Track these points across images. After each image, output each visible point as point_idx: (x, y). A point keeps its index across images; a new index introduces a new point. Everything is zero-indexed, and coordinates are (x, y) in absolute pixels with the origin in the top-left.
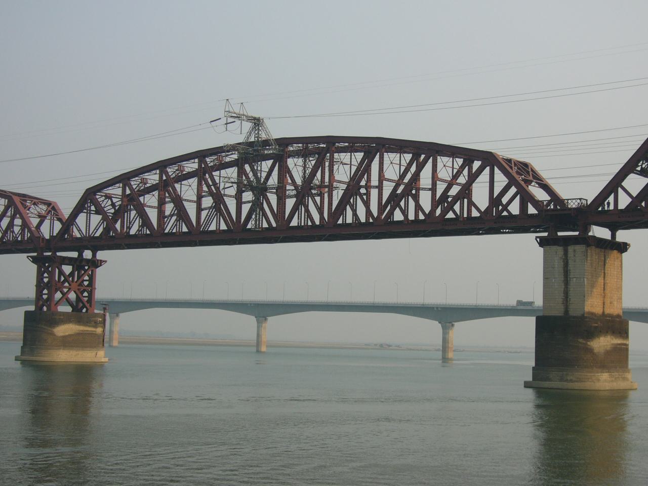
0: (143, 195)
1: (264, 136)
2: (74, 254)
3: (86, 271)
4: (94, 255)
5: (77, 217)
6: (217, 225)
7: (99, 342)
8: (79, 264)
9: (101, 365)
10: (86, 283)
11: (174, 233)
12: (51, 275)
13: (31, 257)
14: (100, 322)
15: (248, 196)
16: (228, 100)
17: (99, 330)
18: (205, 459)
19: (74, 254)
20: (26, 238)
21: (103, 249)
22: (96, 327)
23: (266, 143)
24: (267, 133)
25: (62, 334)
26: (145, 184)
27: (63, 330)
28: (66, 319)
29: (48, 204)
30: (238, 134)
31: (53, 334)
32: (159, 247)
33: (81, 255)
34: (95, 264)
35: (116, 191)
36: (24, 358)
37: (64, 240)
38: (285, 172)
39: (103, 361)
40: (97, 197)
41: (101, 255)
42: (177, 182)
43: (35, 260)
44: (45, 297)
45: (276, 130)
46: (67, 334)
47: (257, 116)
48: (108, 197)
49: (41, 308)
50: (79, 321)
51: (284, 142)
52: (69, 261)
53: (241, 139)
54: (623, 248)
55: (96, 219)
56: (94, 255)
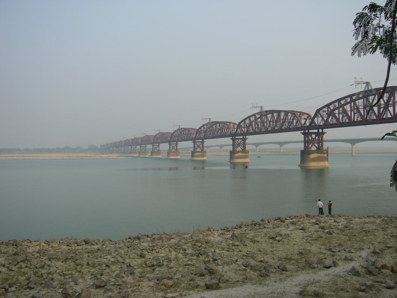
0: (335, 110)
1: (370, 88)
2: (316, 131)
3: (320, 136)
4: (322, 131)
5: (314, 119)
6: (357, 118)
7: (326, 159)
8: (317, 134)
9: (248, 162)
10: (320, 140)
11: (384, 118)
12: (308, 138)
13: (302, 133)
14: (326, 153)
15: (262, 124)
16: (355, 78)
17: (325, 155)
18: (100, 156)
19: (316, 131)
20: (344, 122)
21: (325, 128)
22: (324, 154)
23: (371, 90)
24: (371, 87)
25: (312, 157)
26: (335, 106)
27: (312, 156)
28: (314, 152)
29: (307, 114)
30: (361, 88)
31: (309, 157)
32: (379, 124)
33: (318, 131)
34: (323, 133)
35: (326, 109)
36: (301, 165)
37: (313, 125)
38: (267, 118)
39: (327, 165)
40: (320, 112)
41: (325, 130)
42: (345, 105)
43: (303, 133)
44: (307, 145)
45: (265, 109)
46: (314, 157)
47: (367, 81)
48: (324, 111)
49: (306, 149)
50: (318, 153)
51: (266, 111)
52: (314, 133)
53: (362, 90)
54: (325, 133)
55: (320, 119)
56: (322, 131)
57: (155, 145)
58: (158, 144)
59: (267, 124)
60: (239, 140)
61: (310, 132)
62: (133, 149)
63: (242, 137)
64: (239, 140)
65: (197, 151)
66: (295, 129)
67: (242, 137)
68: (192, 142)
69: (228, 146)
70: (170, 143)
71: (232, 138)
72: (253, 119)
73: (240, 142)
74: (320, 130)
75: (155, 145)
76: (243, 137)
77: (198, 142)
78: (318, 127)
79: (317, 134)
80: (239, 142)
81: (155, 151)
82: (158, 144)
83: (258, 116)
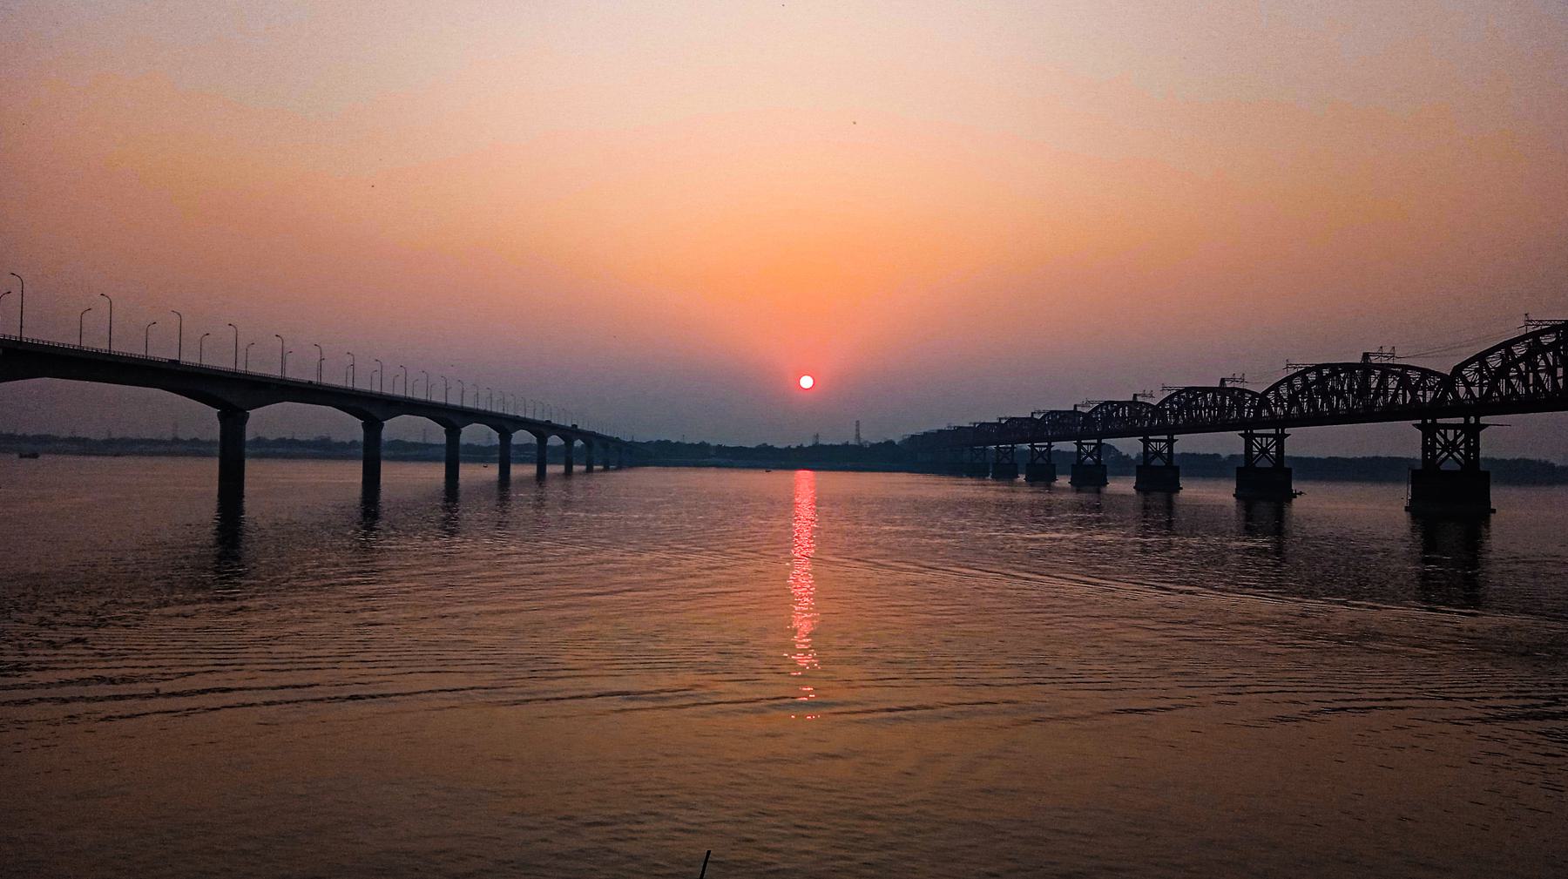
8: (1465, 428)
56: (1477, 420)
57: (1085, 444)
58: (1047, 444)
59: (1205, 413)
60: (1264, 439)
61: (560, 464)
62: (1264, 451)
63: (1273, 431)
64: (1264, 439)
65: (1153, 464)
66: (1393, 413)
67: (1273, 431)
68: (1240, 435)
69: (182, 462)
70: (1079, 441)
71: (1419, 422)
72: (1312, 377)
73: (1268, 445)
74: (1472, 419)
75: (1085, 444)
76: (1277, 431)
77: (1261, 436)
78: (1459, 408)
79: (1465, 428)
80: (1451, 438)
81: (1037, 462)
82: (1047, 444)
83: (1519, 350)
